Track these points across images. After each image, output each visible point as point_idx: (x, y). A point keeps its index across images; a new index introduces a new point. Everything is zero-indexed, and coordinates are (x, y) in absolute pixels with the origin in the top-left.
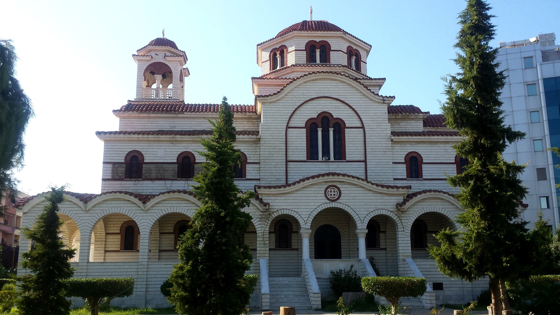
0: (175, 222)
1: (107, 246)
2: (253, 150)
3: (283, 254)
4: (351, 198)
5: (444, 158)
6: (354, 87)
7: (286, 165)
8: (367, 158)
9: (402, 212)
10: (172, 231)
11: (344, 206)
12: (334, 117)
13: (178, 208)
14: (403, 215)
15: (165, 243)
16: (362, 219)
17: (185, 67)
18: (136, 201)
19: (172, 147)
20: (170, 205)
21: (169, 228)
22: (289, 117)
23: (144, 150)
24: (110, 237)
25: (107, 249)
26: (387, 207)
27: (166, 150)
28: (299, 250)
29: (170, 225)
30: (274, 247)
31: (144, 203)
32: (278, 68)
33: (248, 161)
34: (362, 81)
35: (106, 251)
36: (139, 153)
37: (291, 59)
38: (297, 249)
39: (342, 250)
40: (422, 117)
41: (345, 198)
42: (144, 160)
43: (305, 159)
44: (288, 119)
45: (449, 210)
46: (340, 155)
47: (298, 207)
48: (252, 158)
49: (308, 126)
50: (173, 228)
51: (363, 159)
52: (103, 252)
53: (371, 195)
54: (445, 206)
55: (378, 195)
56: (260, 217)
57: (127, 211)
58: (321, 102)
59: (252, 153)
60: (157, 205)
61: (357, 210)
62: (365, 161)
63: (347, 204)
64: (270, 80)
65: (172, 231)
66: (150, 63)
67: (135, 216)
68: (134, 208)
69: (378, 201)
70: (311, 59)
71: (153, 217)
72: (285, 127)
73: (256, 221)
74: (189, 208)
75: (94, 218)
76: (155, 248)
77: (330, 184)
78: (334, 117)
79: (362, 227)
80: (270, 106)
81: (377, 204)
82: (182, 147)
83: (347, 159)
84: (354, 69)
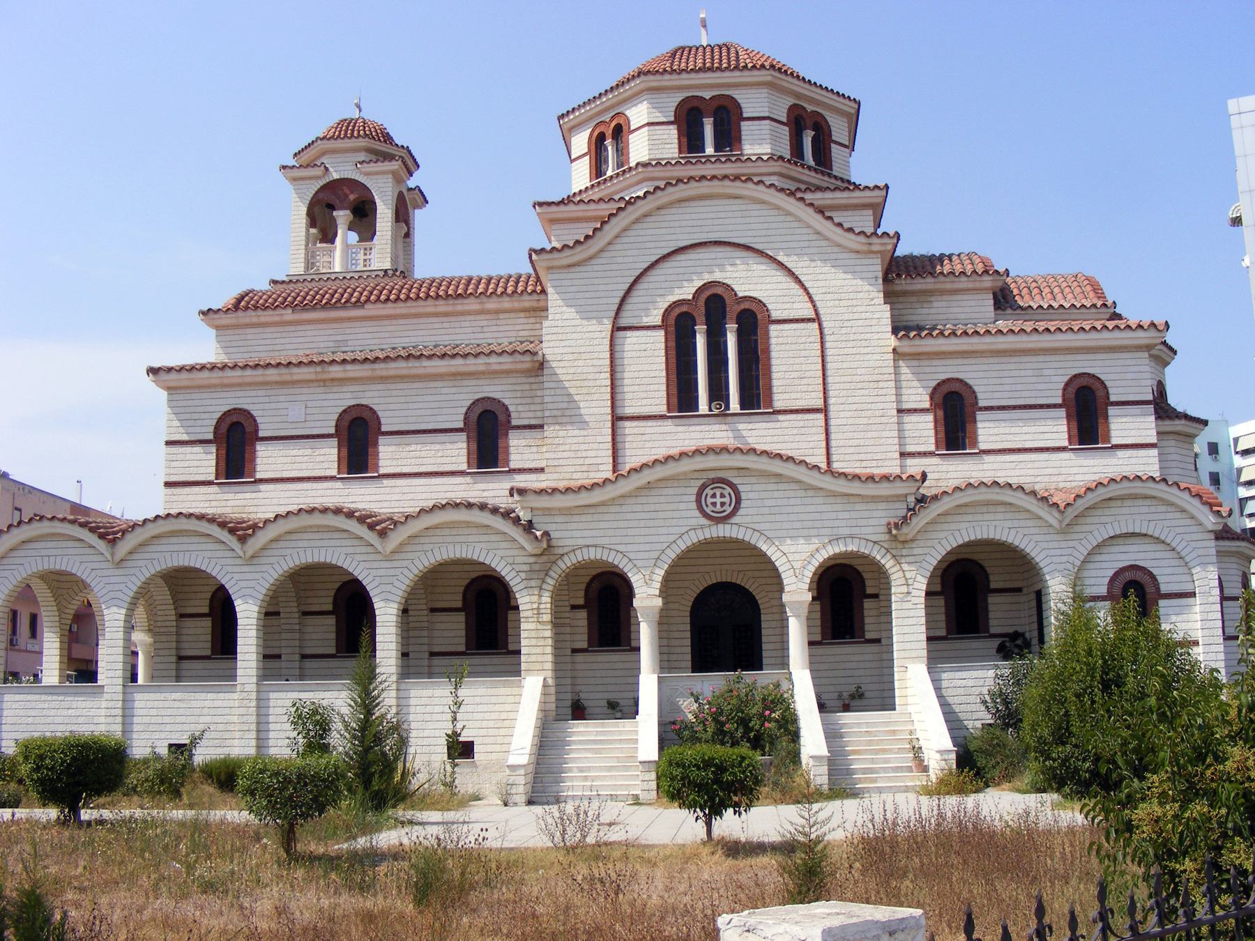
0: (337, 586)
1: (184, 645)
2: (527, 394)
3: (846, 653)
4: (766, 510)
5: (1034, 394)
6: (789, 214)
7: (613, 425)
8: (831, 401)
9: (903, 542)
10: (330, 607)
11: (749, 532)
12: (740, 294)
13: (65, 559)
14: (904, 552)
15: (314, 636)
16: (797, 565)
17: (412, 183)
18: (223, 535)
19: (324, 396)
20: (305, 544)
21: (322, 600)
22: (618, 300)
23: (258, 406)
24: (189, 623)
25: (183, 653)
26: (864, 530)
27: (310, 404)
28: (882, 642)
29: (323, 593)
30: (943, 633)
31: (243, 539)
32: (609, 173)
33: (514, 423)
34: (809, 196)
35: (181, 658)
36: (247, 414)
37: (639, 148)
38: (878, 641)
39: (764, 647)
40: (988, 284)
41: (751, 511)
42: (257, 431)
43: (662, 409)
44: (616, 307)
45: (1026, 531)
46: (755, 395)
47: (627, 540)
48: (523, 415)
49: (672, 321)
50: (330, 600)
51: (819, 403)
52: (174, 659)
53: (820, 500)
54: (1016, 523)
55: (839, 500)
56: (526, 568)
57: (206, 561)
58: (701, 256)
59: (523, 401)
60: (274, 545)
61: (630, 548)
62: (825, 410)
63: (756, 527)
64: (592, 206)
65: (459, 604)
66: (322, 183)
67: (223, 572)
68: (220, 554)
69: (841, 515)
70: (691, 142)
71: (265, 575)
72: (832, 408)
73: (518, 580)
74: (350, 550)
75: (406, 571)
76: (289, 650)
77: (712, 475)
78: (690, 297)
79: (797, 591)
80: (570, 275)
81: (836, 523)
82: (349, 395)
83: (779, 403)
84: (812, 163)
